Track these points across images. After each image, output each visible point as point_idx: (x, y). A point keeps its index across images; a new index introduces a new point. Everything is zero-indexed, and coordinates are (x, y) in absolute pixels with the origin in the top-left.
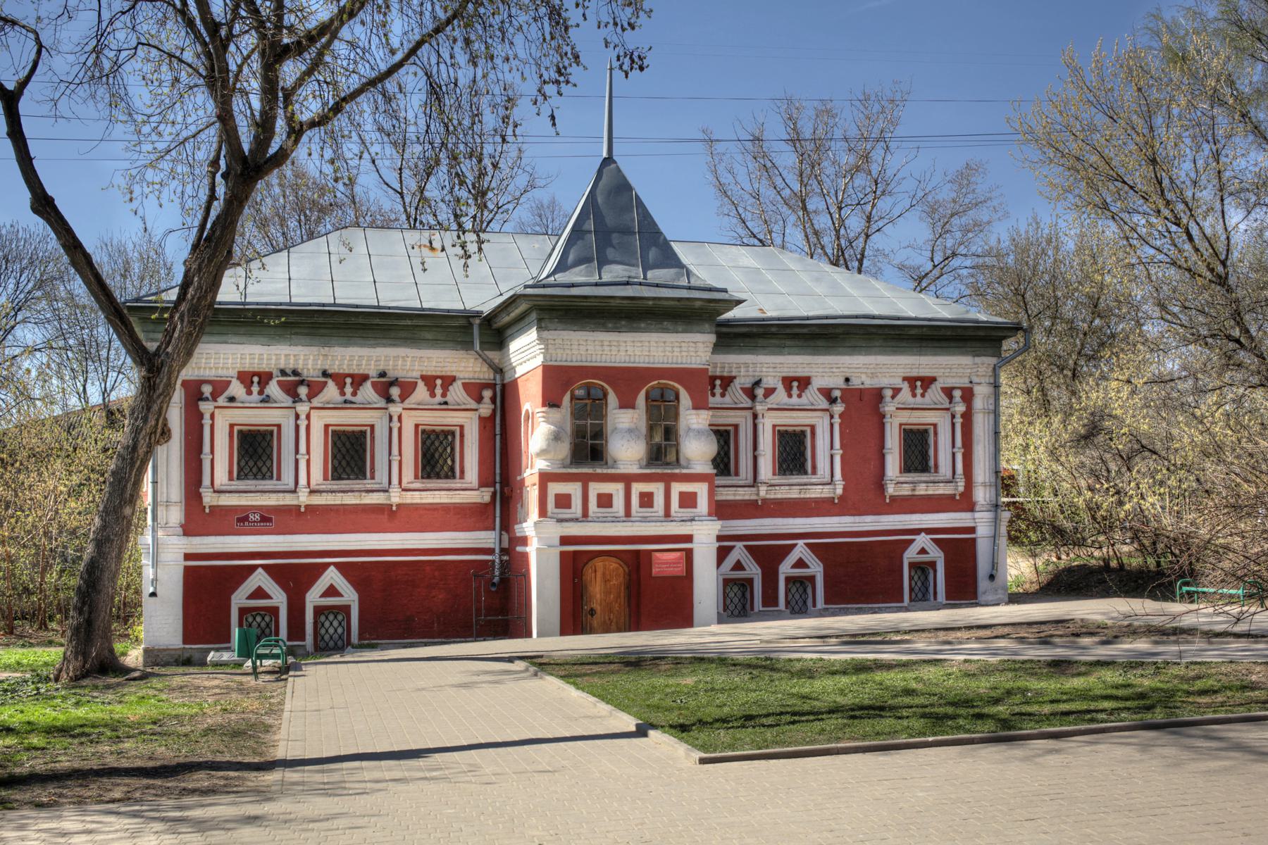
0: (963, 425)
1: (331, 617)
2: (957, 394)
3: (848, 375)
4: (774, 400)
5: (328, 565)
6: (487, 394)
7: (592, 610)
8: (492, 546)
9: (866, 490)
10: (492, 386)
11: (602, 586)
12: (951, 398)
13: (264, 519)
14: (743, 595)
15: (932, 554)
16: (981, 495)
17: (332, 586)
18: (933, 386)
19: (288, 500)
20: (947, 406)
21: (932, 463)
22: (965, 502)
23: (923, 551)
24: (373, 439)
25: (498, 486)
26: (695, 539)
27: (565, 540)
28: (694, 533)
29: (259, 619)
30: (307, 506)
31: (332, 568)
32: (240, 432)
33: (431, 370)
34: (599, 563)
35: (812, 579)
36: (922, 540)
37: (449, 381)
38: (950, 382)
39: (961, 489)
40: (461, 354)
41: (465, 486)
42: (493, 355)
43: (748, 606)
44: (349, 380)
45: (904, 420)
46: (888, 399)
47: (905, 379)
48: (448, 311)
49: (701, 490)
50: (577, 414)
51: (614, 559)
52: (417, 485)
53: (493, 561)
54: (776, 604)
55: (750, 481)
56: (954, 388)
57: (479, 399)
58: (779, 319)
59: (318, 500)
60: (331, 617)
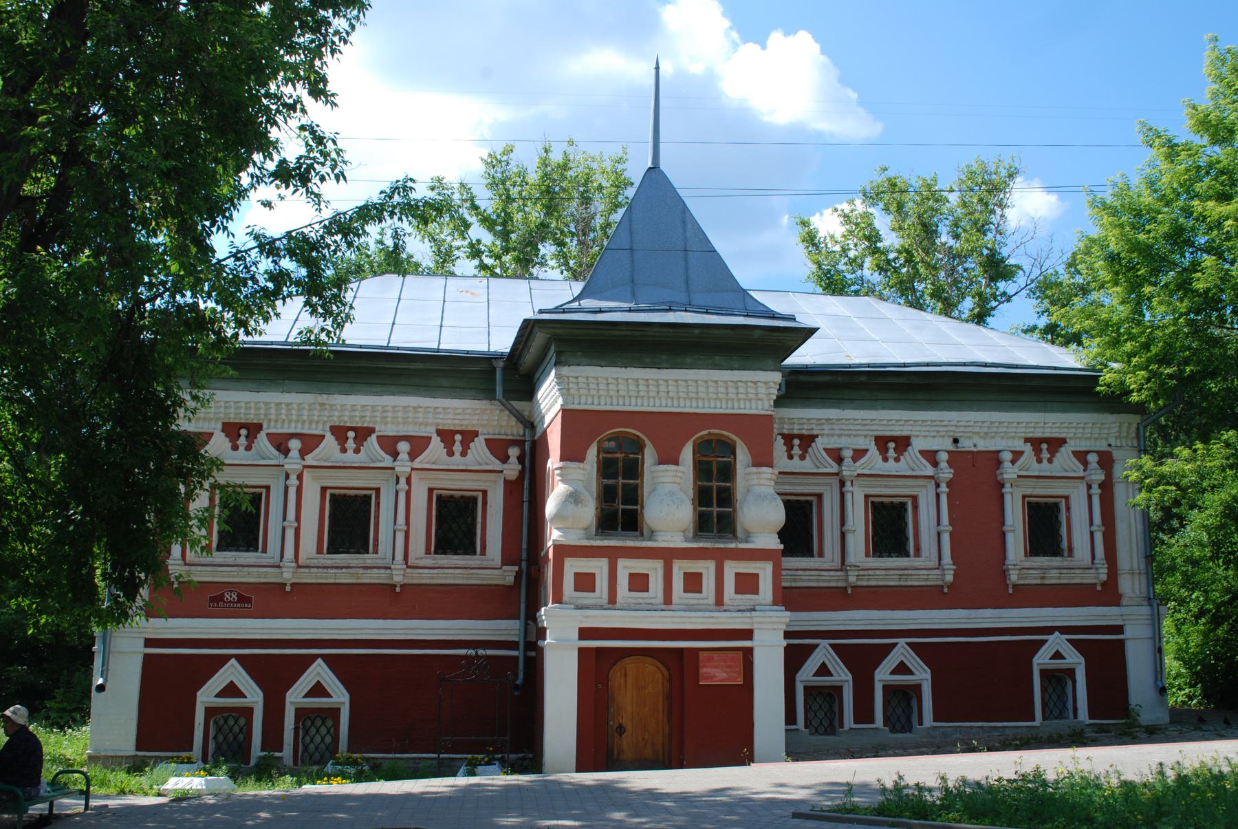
0: (1101, 497)
1: (318, 722)
2: (1093, 459)
3: (957, 435)
4: (862, 466)
5: (228, 657)
6: (514, 452)
7: (620, 726)
8: (516, 639)
9: (979, 578)
10: (519, 443)
11: (637, 697)
12: (1085, 464)
13: (242, 599)
14: (831, 707)
15: (1069, 660)
16: (1130, 585)
17: (1057, 652)
18: (1062, 449)
19: (270, 576)
20: (1082, 474)
21: (1065, 545)
22: (1108, 594)
23: (1057, 655)
24: (378, 504)
25: (524, 564)
26: (756, 635)
27: (585, 633)
28: (755, 626)
29: (231, 722)
30: (293, 585)
31: (319, 661)
32: (439, 497)
33: (449, 423)
34: (630, 664)
35: (917, 688)
36: (1056, 642)
37: (469, 436)
38: (1083, 446)
39: (1104, 577)
40: (484, 404)
41: (485, 564)
42: (518, 405)
43: (836, 723)
44: (351, 434)
45: (1029, 492)
46: (1007, 465)
47: (1027, 440)
48: (468, 352)
49: (765, 571)
50: (606, 468)
51: (649, 660)
52: (428, 561)
53: (516, 658)
54: (872, 721)
55: (837, 563)
56: (1088, 452)
57: (505, 459)
58: (869, 366)
59: (308, 577)
60: (318, 722)
